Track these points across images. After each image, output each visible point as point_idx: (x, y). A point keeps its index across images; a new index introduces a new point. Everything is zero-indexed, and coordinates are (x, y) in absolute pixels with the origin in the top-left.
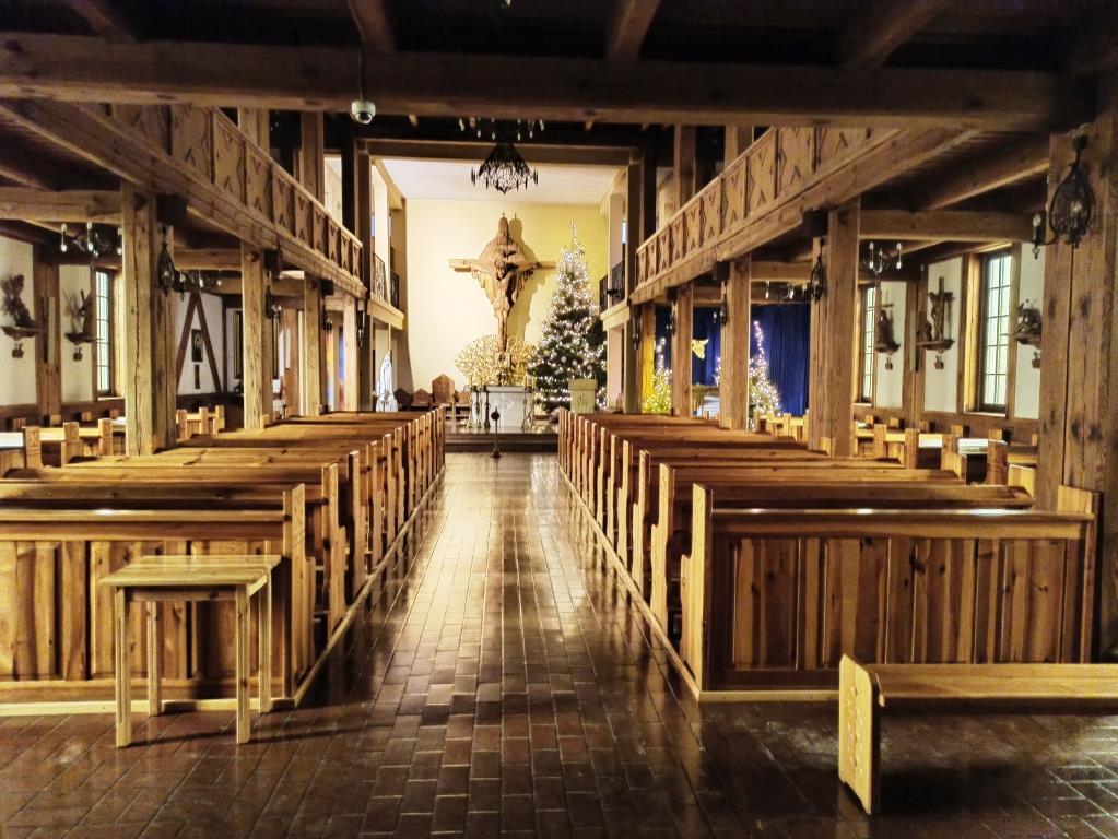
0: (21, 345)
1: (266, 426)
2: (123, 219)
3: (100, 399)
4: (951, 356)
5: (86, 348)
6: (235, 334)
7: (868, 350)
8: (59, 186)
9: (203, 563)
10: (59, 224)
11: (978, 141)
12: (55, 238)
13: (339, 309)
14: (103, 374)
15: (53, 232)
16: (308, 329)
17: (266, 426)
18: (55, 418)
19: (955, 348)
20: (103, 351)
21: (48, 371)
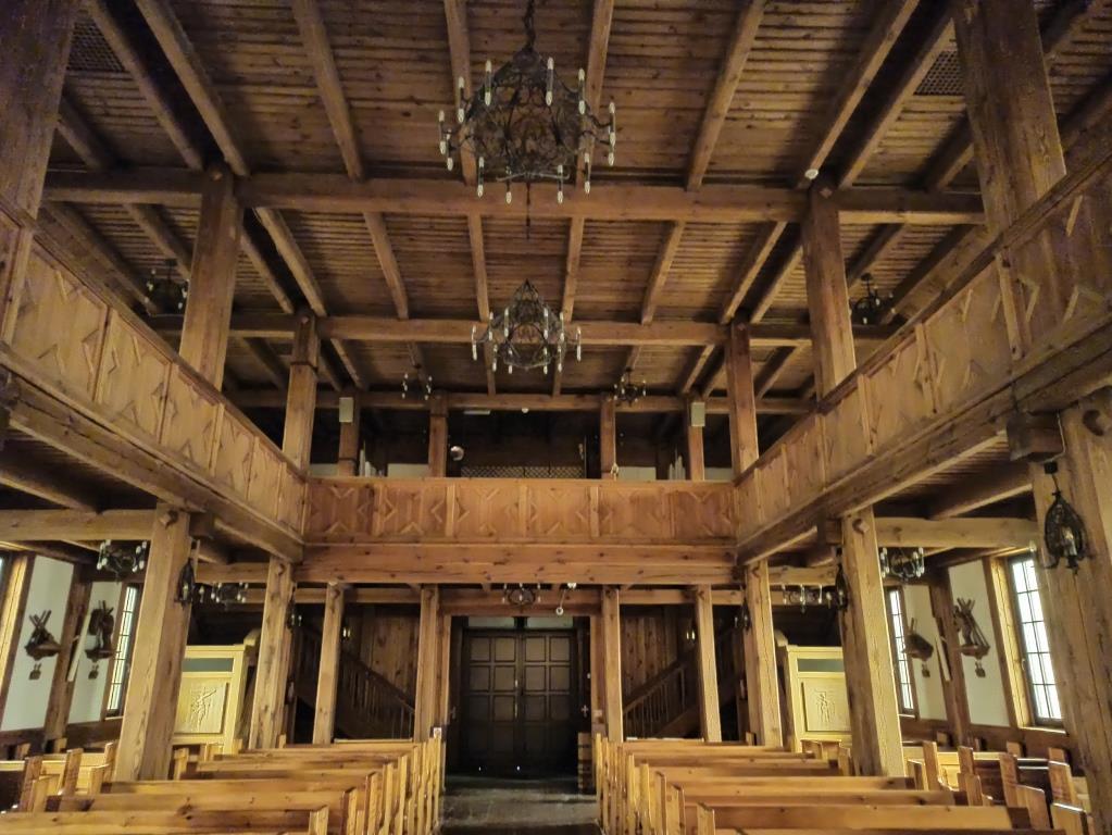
0: (97, 667)
1: (915, 93)
2: (154, 534)
3: (107, 719)
4: (990, 662)
5: (103, 663)
6: (738, 753)
7: (901, 656)
8: (100, 507)
9: (636, 251)
10: (98, 543)
11: (995, 450)
12: (95, 557)
13: (461, 213)
14: (116, 691)
15: (92, 551)
16: (173, 474)
17: (915, 93)
18: (61, 743)
19: (993, 653)
20: (120, 666)
21: (62, 692)
